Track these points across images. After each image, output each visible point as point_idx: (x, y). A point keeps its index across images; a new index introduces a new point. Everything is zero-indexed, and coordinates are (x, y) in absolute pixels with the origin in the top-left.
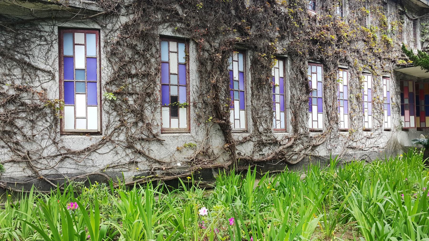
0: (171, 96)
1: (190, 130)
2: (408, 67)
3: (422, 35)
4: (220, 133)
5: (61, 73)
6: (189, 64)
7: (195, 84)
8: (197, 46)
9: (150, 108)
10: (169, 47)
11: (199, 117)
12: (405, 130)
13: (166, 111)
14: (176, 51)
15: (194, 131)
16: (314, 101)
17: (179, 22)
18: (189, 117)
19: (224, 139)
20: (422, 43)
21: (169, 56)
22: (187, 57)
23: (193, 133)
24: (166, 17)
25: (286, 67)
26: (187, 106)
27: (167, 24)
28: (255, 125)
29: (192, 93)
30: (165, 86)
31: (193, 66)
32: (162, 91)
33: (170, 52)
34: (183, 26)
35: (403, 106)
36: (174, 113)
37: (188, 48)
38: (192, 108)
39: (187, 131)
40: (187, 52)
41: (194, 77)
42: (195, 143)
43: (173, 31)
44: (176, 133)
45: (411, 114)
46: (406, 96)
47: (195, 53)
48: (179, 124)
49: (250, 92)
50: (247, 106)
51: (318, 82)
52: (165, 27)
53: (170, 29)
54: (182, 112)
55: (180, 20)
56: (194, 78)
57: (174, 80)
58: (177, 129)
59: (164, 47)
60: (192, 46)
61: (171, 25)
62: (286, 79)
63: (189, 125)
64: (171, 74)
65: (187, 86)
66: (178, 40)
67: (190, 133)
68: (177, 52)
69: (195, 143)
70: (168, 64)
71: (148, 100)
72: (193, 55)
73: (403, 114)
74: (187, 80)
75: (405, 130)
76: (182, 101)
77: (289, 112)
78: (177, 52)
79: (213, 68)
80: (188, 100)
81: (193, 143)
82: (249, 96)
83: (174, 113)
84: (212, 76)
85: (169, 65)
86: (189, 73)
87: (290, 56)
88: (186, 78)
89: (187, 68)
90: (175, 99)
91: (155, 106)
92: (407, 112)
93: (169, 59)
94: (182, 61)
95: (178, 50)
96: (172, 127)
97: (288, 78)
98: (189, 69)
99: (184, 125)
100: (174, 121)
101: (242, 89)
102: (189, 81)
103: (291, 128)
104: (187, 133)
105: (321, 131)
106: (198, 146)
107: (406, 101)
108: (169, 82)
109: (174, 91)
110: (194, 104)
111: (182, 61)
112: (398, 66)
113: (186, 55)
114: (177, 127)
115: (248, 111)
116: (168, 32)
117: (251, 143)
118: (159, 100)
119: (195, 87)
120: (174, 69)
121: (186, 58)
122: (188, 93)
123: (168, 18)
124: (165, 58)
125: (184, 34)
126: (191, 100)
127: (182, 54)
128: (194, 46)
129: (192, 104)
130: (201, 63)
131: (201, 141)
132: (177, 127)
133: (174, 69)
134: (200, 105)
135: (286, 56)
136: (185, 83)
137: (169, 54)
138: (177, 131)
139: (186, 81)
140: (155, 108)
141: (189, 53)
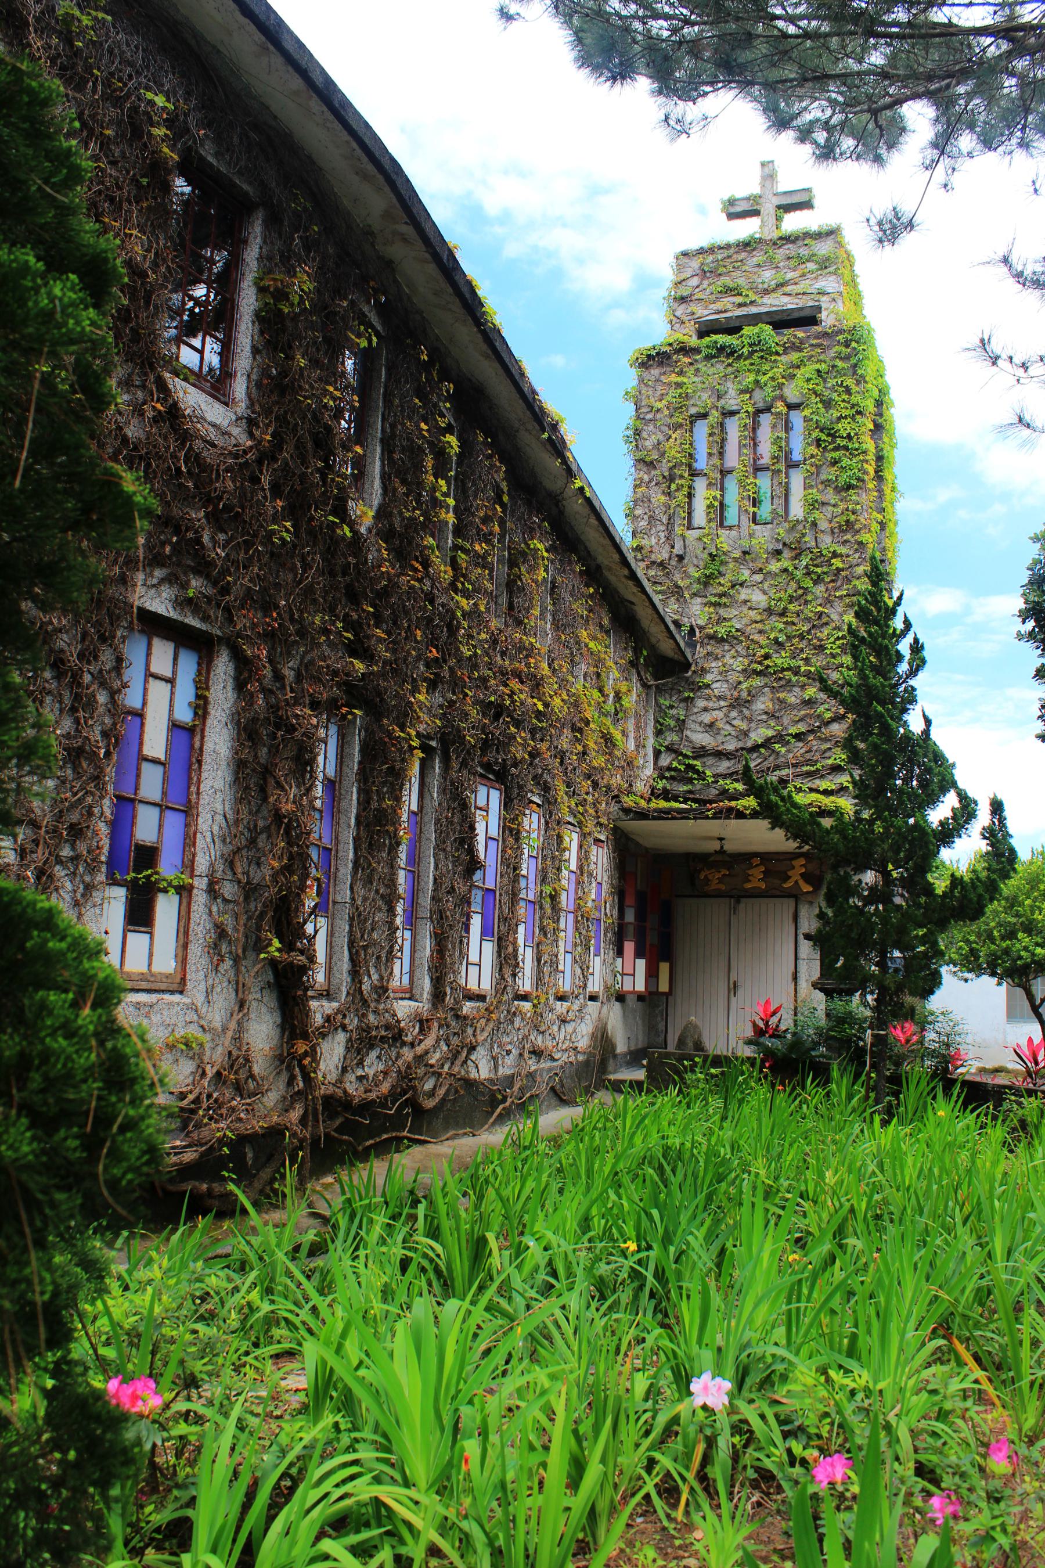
0: (137, 845)
1: (183, 979)
2: (654, 818)
3: (658, 733)
4: (270, 999)
5: (350, 743)
6: (203, 731)
7: (219, 807)
8: (238, 671)
9: (69, 886)
10: (149, 654)
11: (221, 933)
12: (621, 998)
13: (115, 902)
14: (169, 675)
15: (202, 987)
16: (477, 897)
17: (197, 572)
18: (186, 933)
19: (279, 1021)
20: (657, 754)
21: (145, 690)
22: (201, 706)
23: (196, 993)
24: (163, 544)
25: (427, 780)
26: (184, 891)
27: (159, 573)
28: (355, 973)
29: (209, 839)
30: (126, 804)
31: (218, 741)
32: (115, 825)
33: (149, 675)
34: (210, 591)
35: (621, 926)
36: (140, 916)
37: (208, 672)
38: (200, 898)
39: (175, 987)
40: (202, 685)
41: (215, 784)
42: (200, 1035)
43: (183, 603)
44: (138, 991)
45: (638, 954)
46: (630, 900)
47: (231, 694)
48: (151, 955)
49: (351, 855)
50: (335, 903)
51: (489, 838)
52: (155, 581)
53: (167, 592)
54: (166, 909)
55: (203, 567)
56: (219, 784)
57: (152, 784)
58: (143, 977)
59: (134, 650)
60: (223, 667)
61: (170, 580)
62: (426, 819)
63: (183, 960)
64: (146, 759)
65: (188, 810)
66: (181, 636)
67: (181, 992)
68: (171, 681)
69: (200, 1035)
70: (138, 720)
71: (66, 852)
72: (223, 697)
73: (620, 953)
74: (193, 789)
75: (621, 998)
76: (167, 868)
77: (426, 930)
78: (171, 681)
79: (269, 753)
80: (189, 866)
81: (194, 1031)
82: (345, 871)
83: (140, 916)
84: (279, 785)
85: (142, 725)
86: (200, 762)
87: (445, 745)
88: (190, 778)
89: (197, 745)
90: (147, 856)
91: (87, 879)
92: (629, 947)
93: (144, 703)
94: (184, 715)
95: (174, 672)
96: (155, 969)
97: (430, 817)
98: (201, 749)
99: (166, 964)
100: (138, 941)
101: (326, 842)
102: (198, 793)
103: (426, 984)
104: (172, 992)
105: (481, 998)
106: (207, 1046)
107: (630, 917)
108: (137, 789)
109: (146, 827)
110: (211, 884)
111: (184, 715)
112: (627, 811)
113: (198, 697)
114: (145, 970)
115: (338, 922)
116: (160, 603)
117: (341, 1037)
118: (103, 859)
119: (219, 818)
120: (155, 741)
121: (197, 707)
122: (189, 840)
123: (168, 549)
124: (132, 699)
125: (205, 619)
126: (202, 864)
127: (186, 691)
128: (231, 668)
129: (200, 883)
130: (247, 731)
131: (217, 1024)
132: (145, 970)
133: (155, 741)
134: (228, 890)
135: (433, 744)
136: (184, 800)
137: (146, 681)
138: (144, 985)
139: (188, 793)
140: (89, 888)
141: (208, 689)
